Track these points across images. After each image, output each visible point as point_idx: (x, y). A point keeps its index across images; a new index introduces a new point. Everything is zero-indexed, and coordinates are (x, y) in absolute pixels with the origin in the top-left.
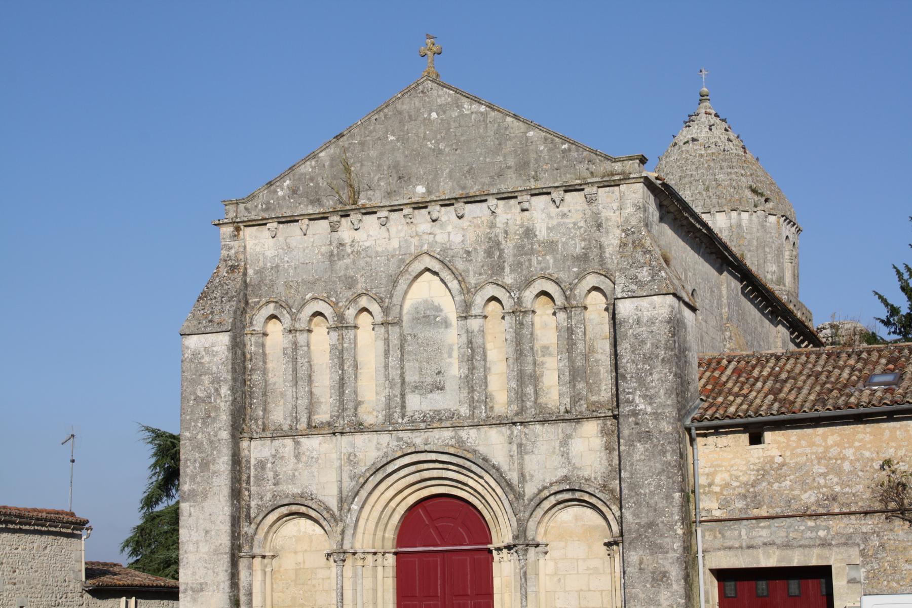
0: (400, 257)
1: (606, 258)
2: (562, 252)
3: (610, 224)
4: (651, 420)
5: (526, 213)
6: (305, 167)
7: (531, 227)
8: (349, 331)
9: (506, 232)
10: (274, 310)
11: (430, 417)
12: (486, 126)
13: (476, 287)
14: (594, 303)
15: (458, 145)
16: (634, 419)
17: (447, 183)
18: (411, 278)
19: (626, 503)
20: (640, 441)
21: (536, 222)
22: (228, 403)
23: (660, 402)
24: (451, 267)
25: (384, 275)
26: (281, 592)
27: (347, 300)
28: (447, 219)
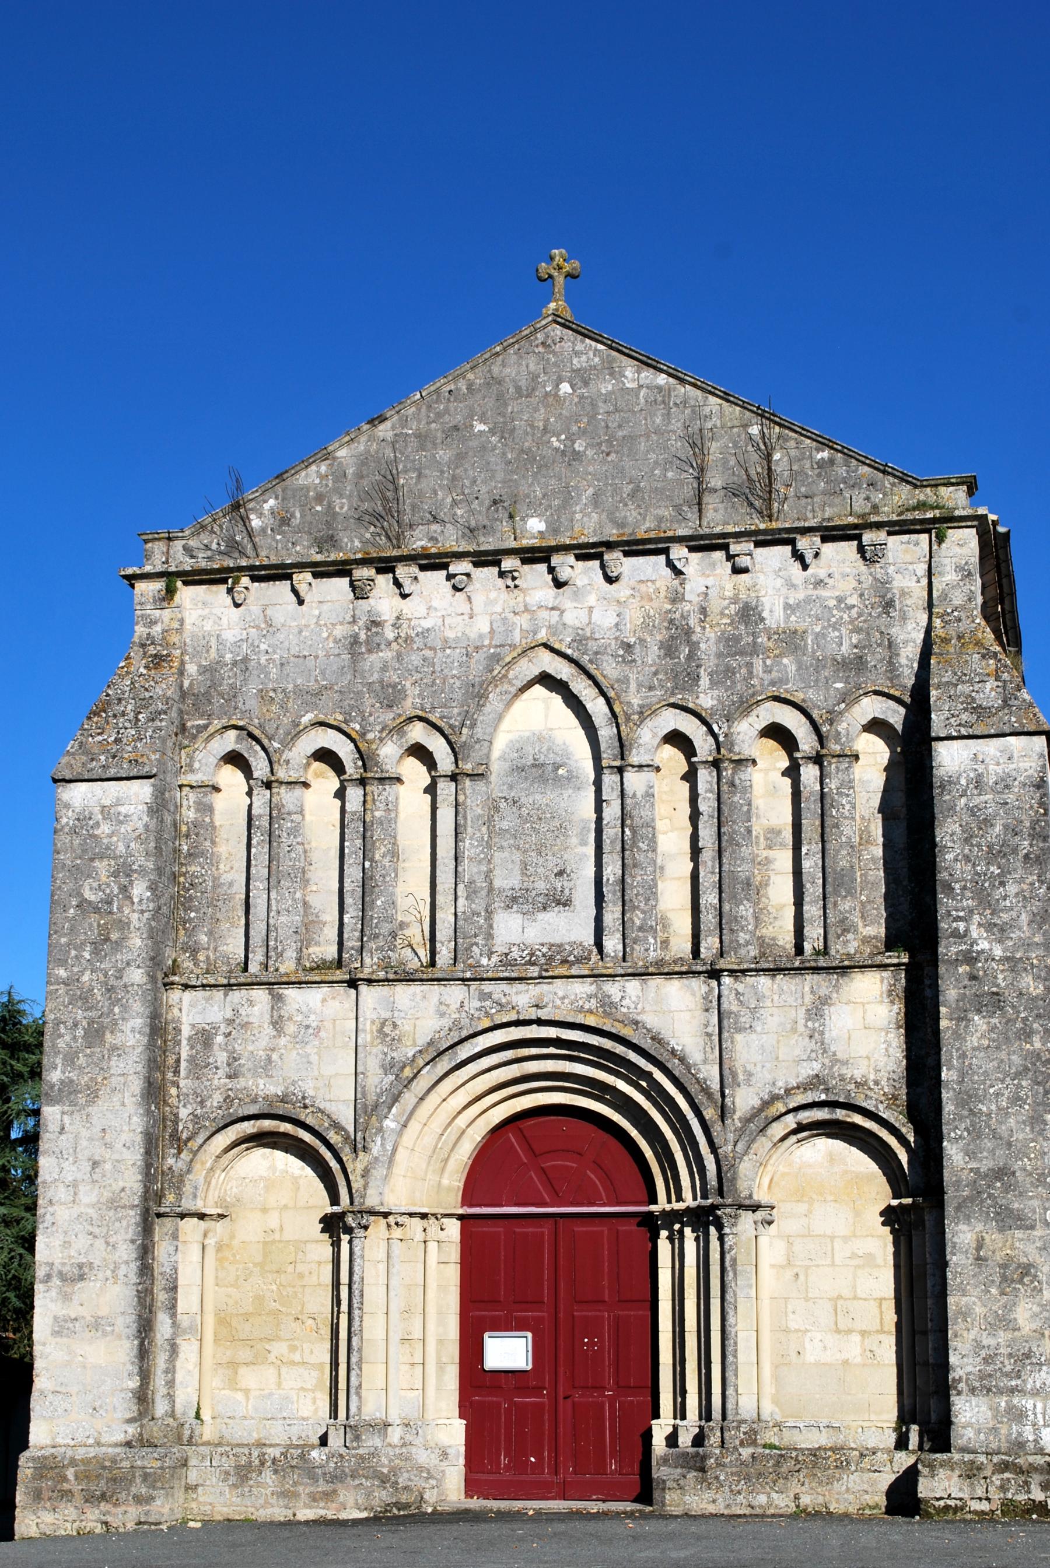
0: (492, 651)
1: (901, 666)
2: (814, 652)
3: (909, 602)
4: (1002, 971)
5: (743, 576)
6: (307, 475)
7: (754, 603)
8: (387, 787)
9: (703, 611)
10: (237, 742)
11: (544, 955)
12: (669, 414)
13: (641, 713)
14: (871, 751)
15: (612, 446)
16: (968, 968)
17: (589, 515)
18: (513, 690)
19: (950, 1130)
20: (979, 1011)
21: (763, 593)
22: (146, 915)
23: (1020, 938)
24: (594, 672)
25: (458, 684)
26: (232, 1286)
27: (383, 729)
28: (587, 582)
